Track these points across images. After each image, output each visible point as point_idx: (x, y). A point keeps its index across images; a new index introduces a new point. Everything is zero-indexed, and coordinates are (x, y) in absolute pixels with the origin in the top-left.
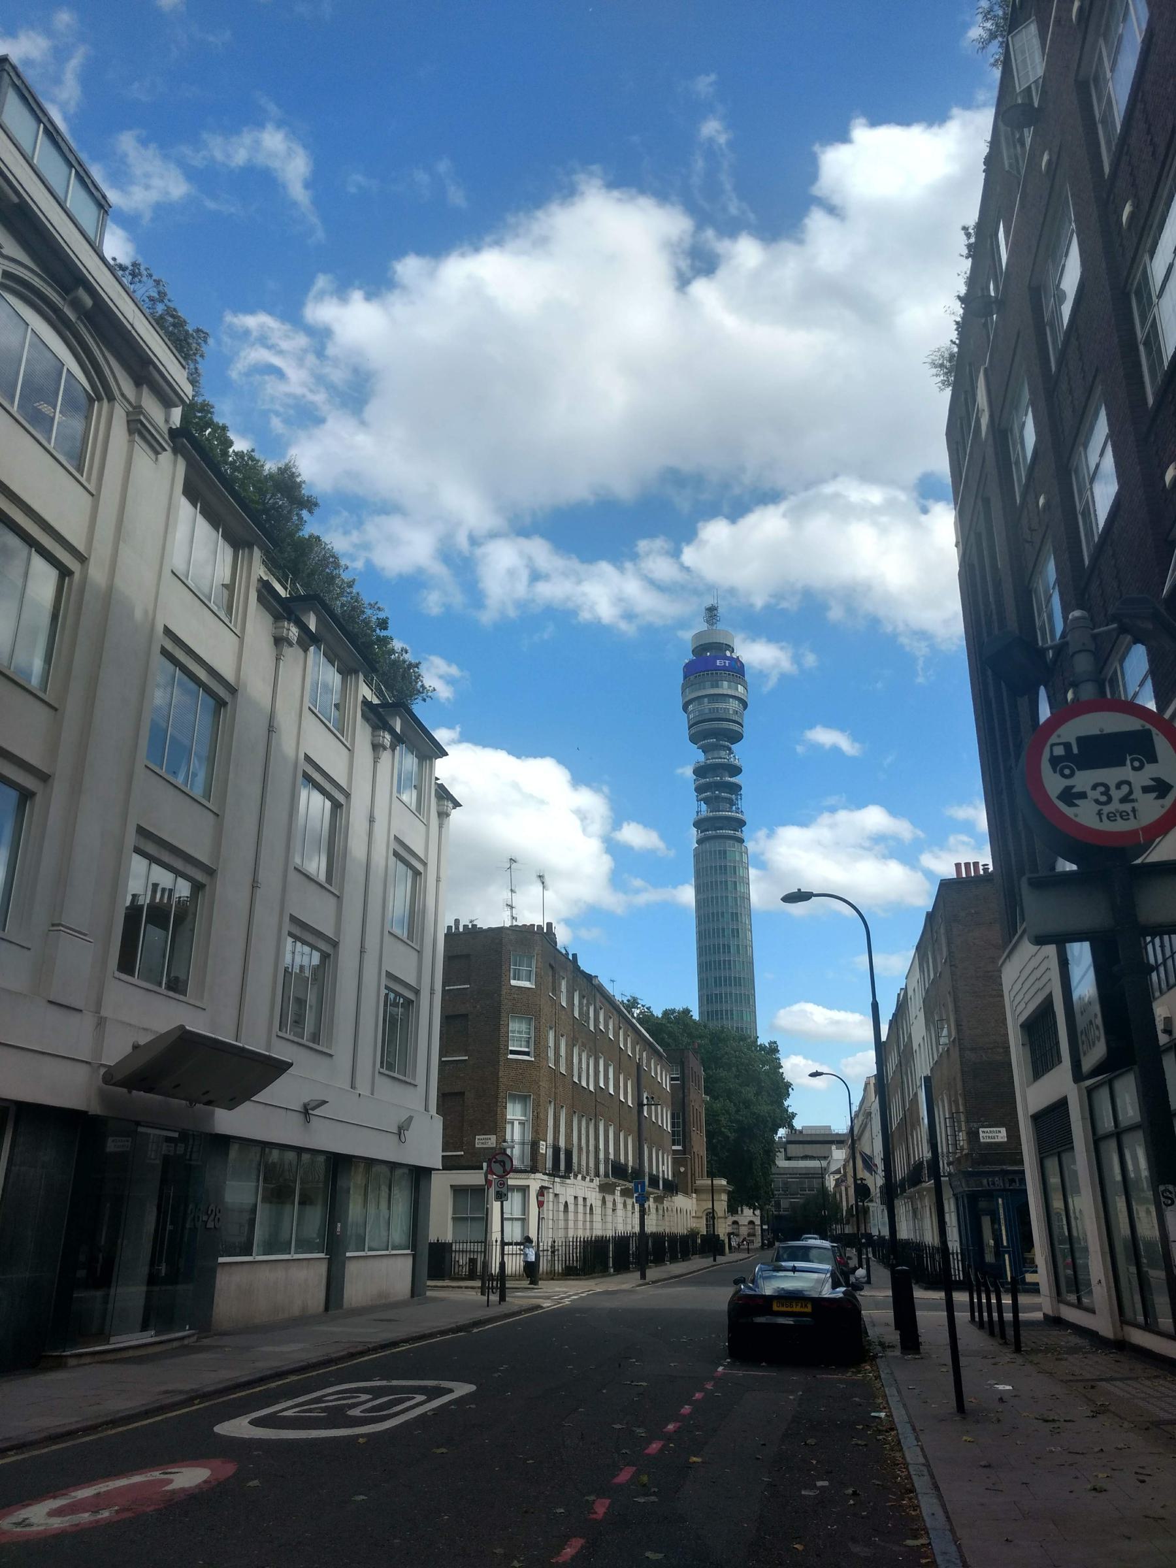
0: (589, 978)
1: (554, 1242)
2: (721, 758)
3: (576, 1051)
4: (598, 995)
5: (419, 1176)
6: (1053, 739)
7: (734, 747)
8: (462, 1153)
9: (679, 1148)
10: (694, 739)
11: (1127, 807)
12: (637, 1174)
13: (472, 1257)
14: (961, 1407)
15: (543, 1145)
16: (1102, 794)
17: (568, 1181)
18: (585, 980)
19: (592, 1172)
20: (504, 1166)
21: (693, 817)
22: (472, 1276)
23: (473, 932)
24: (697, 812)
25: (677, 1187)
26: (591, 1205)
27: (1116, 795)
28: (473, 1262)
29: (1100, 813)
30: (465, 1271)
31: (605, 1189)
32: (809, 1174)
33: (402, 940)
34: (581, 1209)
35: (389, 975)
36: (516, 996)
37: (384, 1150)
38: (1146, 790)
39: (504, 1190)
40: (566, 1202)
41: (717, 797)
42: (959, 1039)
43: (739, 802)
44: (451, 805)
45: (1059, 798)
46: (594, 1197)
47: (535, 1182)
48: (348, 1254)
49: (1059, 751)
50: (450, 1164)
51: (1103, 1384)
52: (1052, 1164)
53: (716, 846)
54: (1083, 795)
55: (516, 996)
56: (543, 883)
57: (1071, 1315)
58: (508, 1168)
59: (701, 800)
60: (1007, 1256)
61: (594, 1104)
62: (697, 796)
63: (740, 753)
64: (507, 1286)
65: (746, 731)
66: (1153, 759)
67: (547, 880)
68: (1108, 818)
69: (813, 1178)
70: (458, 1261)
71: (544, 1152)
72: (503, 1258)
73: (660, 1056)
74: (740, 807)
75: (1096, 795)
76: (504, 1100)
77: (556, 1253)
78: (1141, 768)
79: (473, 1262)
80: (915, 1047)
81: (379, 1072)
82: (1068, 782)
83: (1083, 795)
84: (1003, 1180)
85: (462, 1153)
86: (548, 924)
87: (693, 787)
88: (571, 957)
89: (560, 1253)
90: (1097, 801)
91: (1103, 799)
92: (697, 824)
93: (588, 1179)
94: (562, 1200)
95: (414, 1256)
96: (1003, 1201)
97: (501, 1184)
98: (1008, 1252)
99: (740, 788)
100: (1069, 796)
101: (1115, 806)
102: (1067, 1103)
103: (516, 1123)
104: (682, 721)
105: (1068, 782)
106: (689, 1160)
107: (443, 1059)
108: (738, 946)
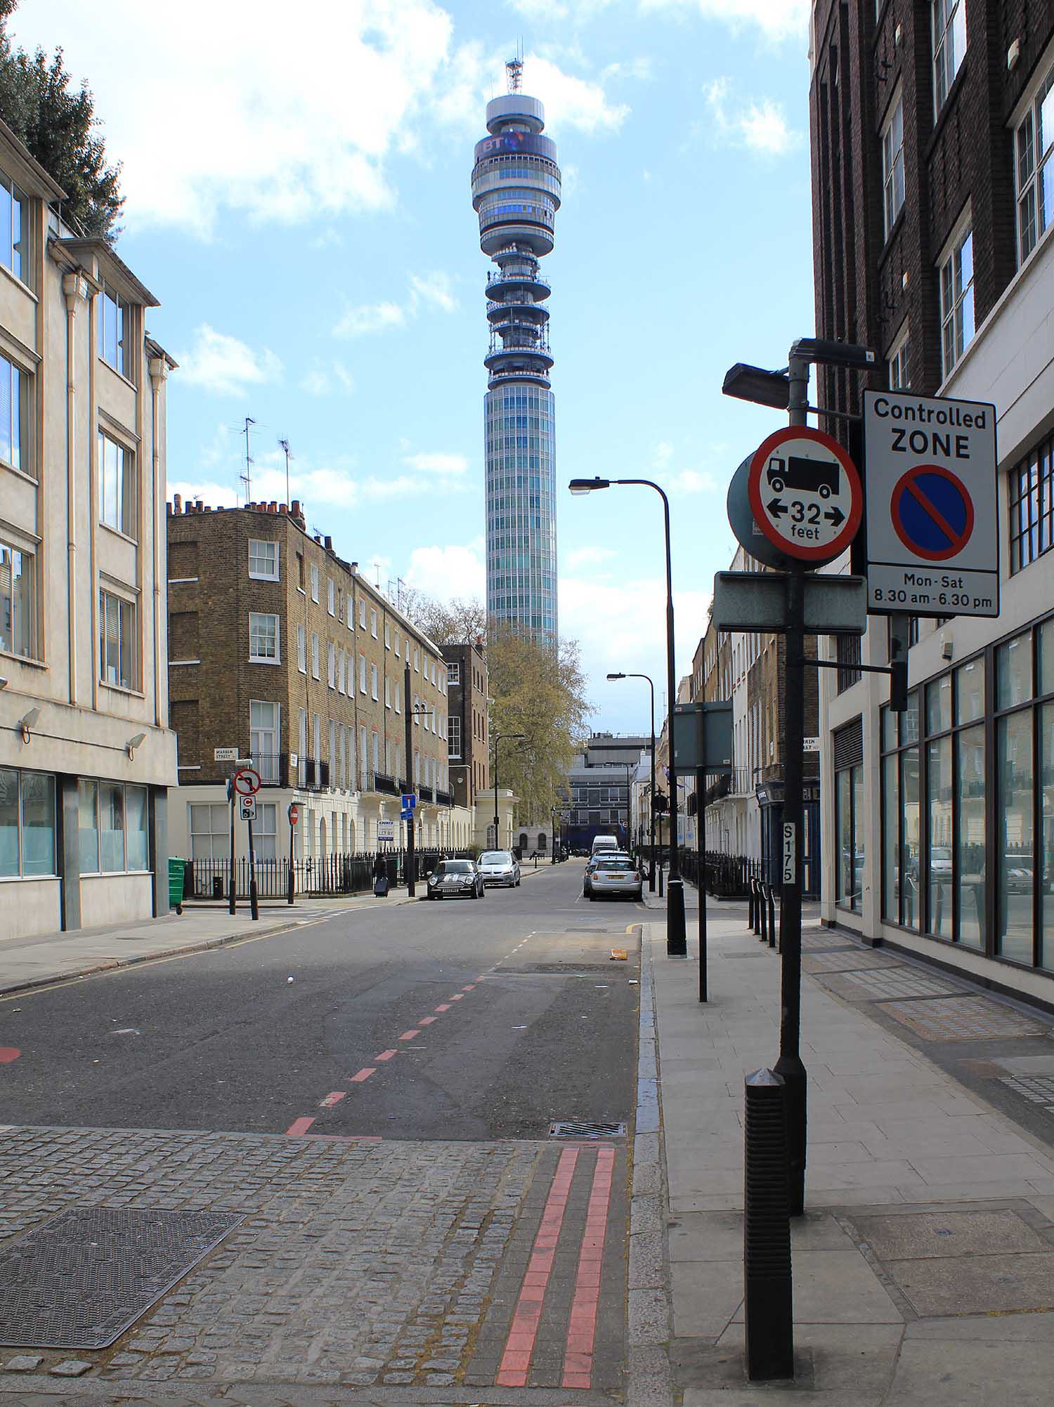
0: (347, 567)
1: (310, 860)
2: (523, 275)
3: (332, 653)
4: (358, 588)
5: (155, 792)
6: (773, 454)
7: (541, 260)
8: (199, 767)
9: (458, 757)
10: (487, 248)
11: (812, 527)
12: (407, 787)
13: (216, 876)
14: (703, 997)
15: (294, 758)
16: (798, 511)
17: (323, 796)
18: (340, 569)
19: (354, 785)
20: (250, 784)
21: (484, 353)
22: (218, 895)
23: (197, 511)
24: (490, 348)
25: (453, 799)
26: (352, 820)
27: (809, 514)
28: (217, 880)
29: (793, 528)
30: (210, 891)
31: (367, 807)
32: (612, 782)
33: (115, 534)
34: (340, 824)
35: (104, 575)
36: (256, 591)
37: (109, 767)
38: (828, 516)
39: (252, 808)
40: (323, 819)
41: (517, 328)
42: (778, 643)
43: (546, 334)
44: (166, 366)
45: (768, 507)
46: (353, 813)
47: (285, 798)
48: (82, 875)
49: (776, 466)
50: (186, 779)
51: (846, 975)
52: (844, 778)
53: (513, 390)
54: (785, 509)
55: (256, 591)
56: (287, 451)
57: (844, 918)
58: (255, 784)
59: (494, 331)
60: (806, 866)
61: (353, 711)
62: (491, 326)
63: (548, 269)
64: (259, 905)
65: (557, 239)
66: (836, 492)
67: (291, 445)
68: (799, 533)
69: (617, 786)
70: (201, 880)
71: (296, 765)
72: (253, 877)
73: (435, 656)
74: (546, 341)
75: (793, 511)
76: (246, 710)
77: (313, 871)
78: (826, 496)
79: (217, 880)
80: (734, 647)
81: (100, 685)
82: (777, 495)
83: (785, 509)
84: (812, 791)
85: (199, 767)
86: (293, 502)
87: (485, 312)
88: (323, 544)
89: (317, 870)
90: (793, 517)
91: (798, 516)
92: (489, 363)
93: (348, 792)
94: (318, 816)
95: (154, 876)
96: (809, 812)
97: (247, 802)
98: (808, 863)
99: (548, 316)
100: (776, 508)
101: (804, 525)
102: (861, 720)
103: (262, 735)
104: (472, 221)
105: (777, 495)
106: (468, 770)
107: (170, 663)
108: (538, 518)
